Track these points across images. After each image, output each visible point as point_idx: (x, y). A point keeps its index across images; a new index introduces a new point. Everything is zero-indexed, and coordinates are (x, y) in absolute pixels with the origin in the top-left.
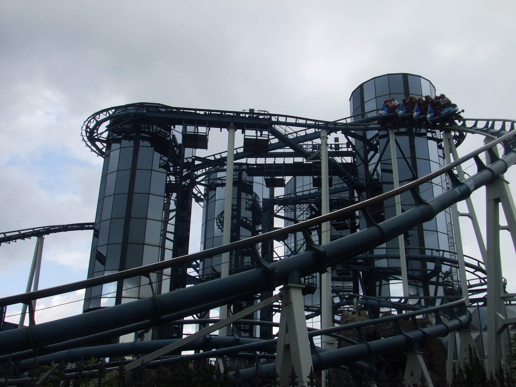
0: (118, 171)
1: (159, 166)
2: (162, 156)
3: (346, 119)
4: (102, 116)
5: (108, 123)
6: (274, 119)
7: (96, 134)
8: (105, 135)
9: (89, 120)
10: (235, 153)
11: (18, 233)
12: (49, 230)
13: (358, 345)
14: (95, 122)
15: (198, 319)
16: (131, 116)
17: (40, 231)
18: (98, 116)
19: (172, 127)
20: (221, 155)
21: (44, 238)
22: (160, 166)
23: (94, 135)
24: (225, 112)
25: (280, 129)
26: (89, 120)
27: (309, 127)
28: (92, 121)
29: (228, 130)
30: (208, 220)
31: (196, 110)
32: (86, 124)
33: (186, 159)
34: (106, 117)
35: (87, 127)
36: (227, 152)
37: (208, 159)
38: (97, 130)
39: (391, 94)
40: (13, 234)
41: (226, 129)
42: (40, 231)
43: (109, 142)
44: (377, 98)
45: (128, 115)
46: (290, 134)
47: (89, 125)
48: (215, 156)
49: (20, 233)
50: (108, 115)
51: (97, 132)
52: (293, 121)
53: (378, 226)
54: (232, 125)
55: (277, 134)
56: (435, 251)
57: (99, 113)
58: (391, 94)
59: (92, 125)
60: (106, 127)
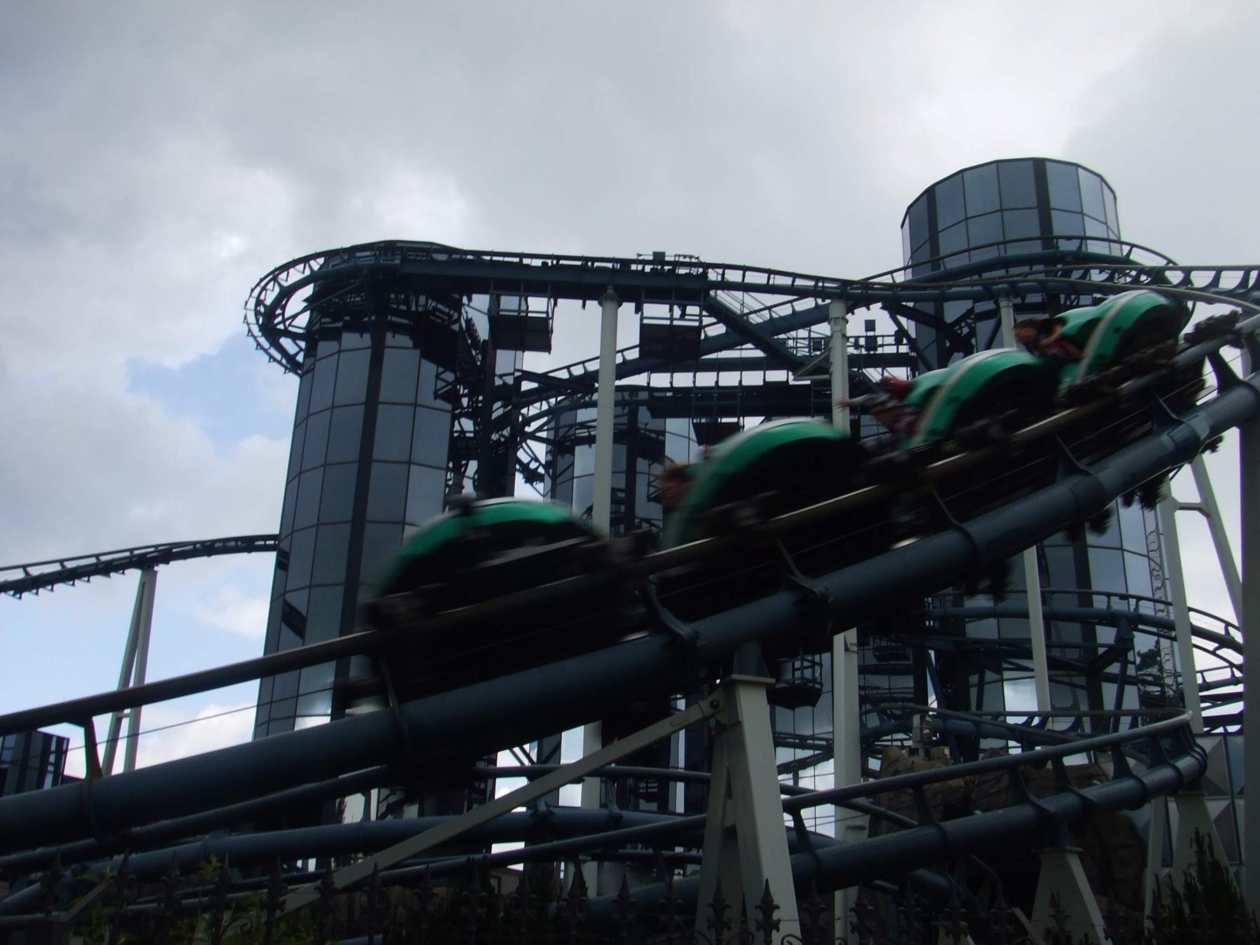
2: (441, 370)
4: (295, 275)
5: (308, 290)
6: (713, 275)
7: (280, 319)
8: (303, 320)
9: (263, 284)
11: (93, 560)
12: (168, 554)
14: (277, 290)
18: (283, 276)
19: (465, 300)
20: (584, 367)
22: (436, 396)
23: (276, 321)
24: (594, 260)
26: (263, 284)
27: (802, 293)
28: (270, 286)
29: (600, 304)
31: (522, 256)
33: (501, 376)
35: (259, 302)
38: (284, 308)
41: (597, 302)
43: (311, 336)
44: (1005, 213)
45: (355, 272)
46: (755, 312)
47: (262, 297)
49: (98, 559)
50: (308, 272)
51: (283, 314)
52: (761, 279)
54: (610, 291)
55: (721, 313)
57: (286, 267)
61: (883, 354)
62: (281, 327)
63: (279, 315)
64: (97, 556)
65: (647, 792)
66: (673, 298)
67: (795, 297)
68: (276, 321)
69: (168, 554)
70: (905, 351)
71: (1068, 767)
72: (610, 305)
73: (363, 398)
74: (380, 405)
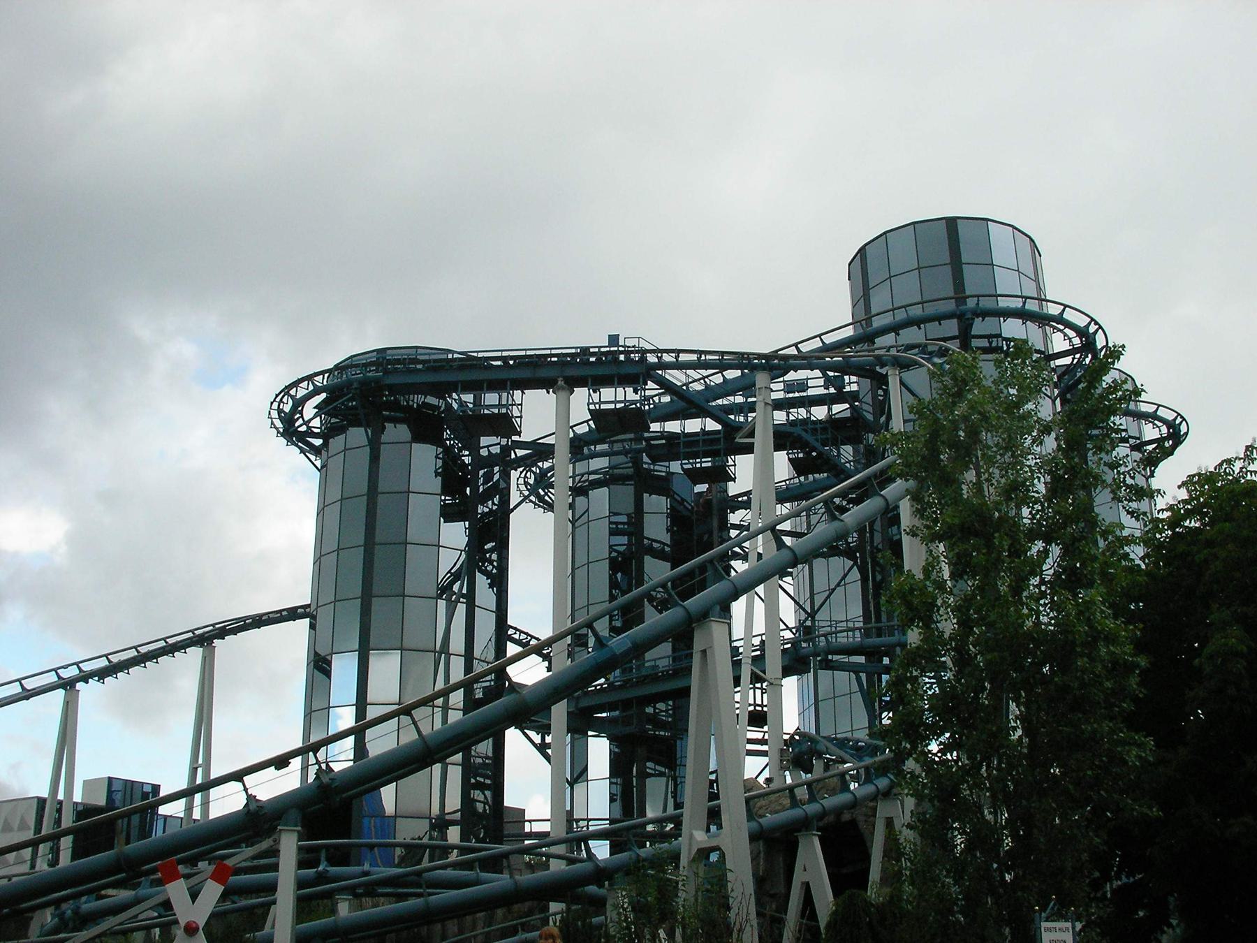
0: (342, 499)
1: (434, 474)
3: (822, 337)
6: (652, 359)
7: (300, 421)
8: (316, 423)
10: (571, 435)
11: (190, 635)
12: (222, 631)
13: (878, 806)
15: (814, 733)
16: (355, 385)
17: (227, 628)
18: (293, 392)
21: (215, 647)
23: (297, 425)
25: (676, 377)
26: (278, 399)
27: (721, 366)
30: (576, 567)
32: (275, 405)
34: (307, 391)
35: (280, 411)
36: (554, 436)
37: (543, 443)
38: (301, 412)
39: (921, 268)
40: (151, 649)
42: (227, 628)
43: (328, 434)
44: (923, 271)
46: (695, 381)
47: (281, 407)
48: (799, 345)
49: (194, 633)
50: (311, 388)
51: (302, 417)
53: (684, 607)
54: (561, 383)
55: (667, 387)
56: (273, 768)
57: (295, 384)
58: (921, 268)
59: (287, 408)
60: (314, 408)
61: (851, 391)
62: (303, 428)
63: (298, 419)
64: (192, 631)
65: (620, 784)
66: (616, 383)
67: (538, 441)
68: (297, 425)
69: (222, 631)
70: (856, 389)
71: (506, 807)
72: (563, 394)
73: (365, 490)
74: (380, 495)
